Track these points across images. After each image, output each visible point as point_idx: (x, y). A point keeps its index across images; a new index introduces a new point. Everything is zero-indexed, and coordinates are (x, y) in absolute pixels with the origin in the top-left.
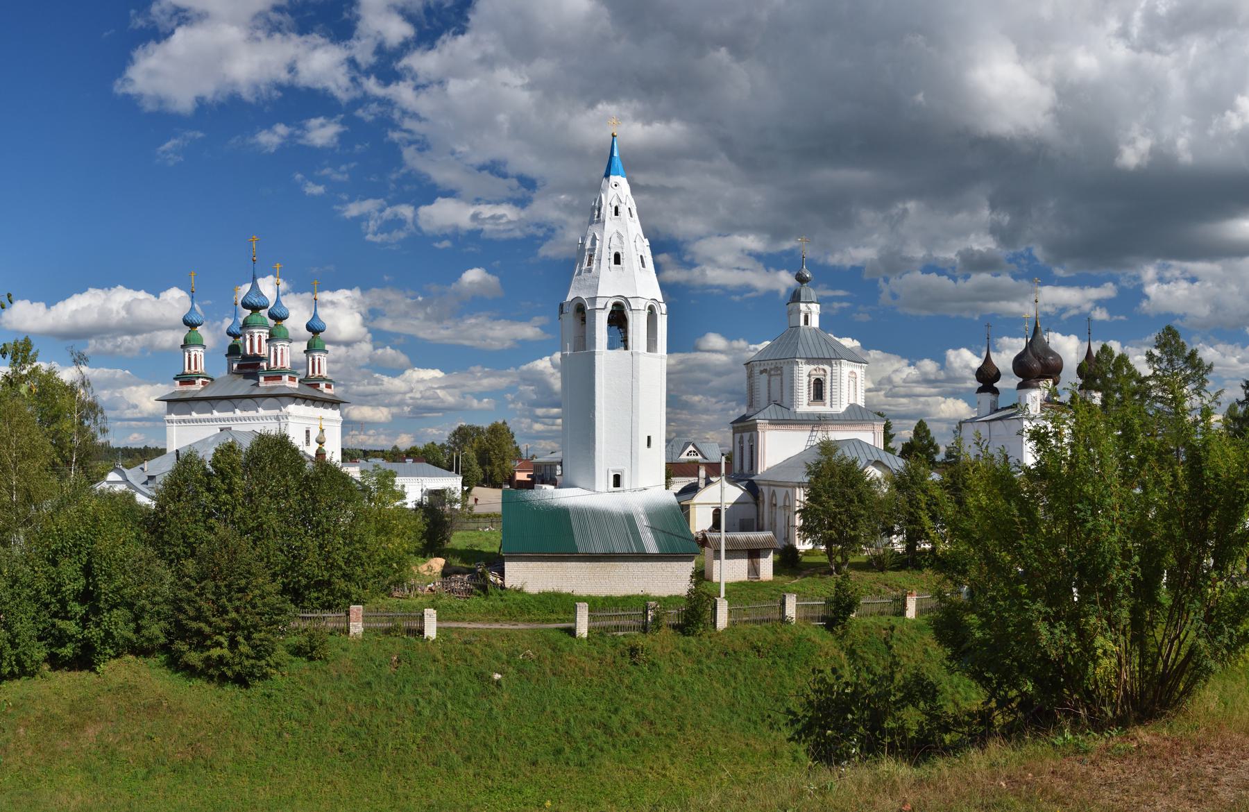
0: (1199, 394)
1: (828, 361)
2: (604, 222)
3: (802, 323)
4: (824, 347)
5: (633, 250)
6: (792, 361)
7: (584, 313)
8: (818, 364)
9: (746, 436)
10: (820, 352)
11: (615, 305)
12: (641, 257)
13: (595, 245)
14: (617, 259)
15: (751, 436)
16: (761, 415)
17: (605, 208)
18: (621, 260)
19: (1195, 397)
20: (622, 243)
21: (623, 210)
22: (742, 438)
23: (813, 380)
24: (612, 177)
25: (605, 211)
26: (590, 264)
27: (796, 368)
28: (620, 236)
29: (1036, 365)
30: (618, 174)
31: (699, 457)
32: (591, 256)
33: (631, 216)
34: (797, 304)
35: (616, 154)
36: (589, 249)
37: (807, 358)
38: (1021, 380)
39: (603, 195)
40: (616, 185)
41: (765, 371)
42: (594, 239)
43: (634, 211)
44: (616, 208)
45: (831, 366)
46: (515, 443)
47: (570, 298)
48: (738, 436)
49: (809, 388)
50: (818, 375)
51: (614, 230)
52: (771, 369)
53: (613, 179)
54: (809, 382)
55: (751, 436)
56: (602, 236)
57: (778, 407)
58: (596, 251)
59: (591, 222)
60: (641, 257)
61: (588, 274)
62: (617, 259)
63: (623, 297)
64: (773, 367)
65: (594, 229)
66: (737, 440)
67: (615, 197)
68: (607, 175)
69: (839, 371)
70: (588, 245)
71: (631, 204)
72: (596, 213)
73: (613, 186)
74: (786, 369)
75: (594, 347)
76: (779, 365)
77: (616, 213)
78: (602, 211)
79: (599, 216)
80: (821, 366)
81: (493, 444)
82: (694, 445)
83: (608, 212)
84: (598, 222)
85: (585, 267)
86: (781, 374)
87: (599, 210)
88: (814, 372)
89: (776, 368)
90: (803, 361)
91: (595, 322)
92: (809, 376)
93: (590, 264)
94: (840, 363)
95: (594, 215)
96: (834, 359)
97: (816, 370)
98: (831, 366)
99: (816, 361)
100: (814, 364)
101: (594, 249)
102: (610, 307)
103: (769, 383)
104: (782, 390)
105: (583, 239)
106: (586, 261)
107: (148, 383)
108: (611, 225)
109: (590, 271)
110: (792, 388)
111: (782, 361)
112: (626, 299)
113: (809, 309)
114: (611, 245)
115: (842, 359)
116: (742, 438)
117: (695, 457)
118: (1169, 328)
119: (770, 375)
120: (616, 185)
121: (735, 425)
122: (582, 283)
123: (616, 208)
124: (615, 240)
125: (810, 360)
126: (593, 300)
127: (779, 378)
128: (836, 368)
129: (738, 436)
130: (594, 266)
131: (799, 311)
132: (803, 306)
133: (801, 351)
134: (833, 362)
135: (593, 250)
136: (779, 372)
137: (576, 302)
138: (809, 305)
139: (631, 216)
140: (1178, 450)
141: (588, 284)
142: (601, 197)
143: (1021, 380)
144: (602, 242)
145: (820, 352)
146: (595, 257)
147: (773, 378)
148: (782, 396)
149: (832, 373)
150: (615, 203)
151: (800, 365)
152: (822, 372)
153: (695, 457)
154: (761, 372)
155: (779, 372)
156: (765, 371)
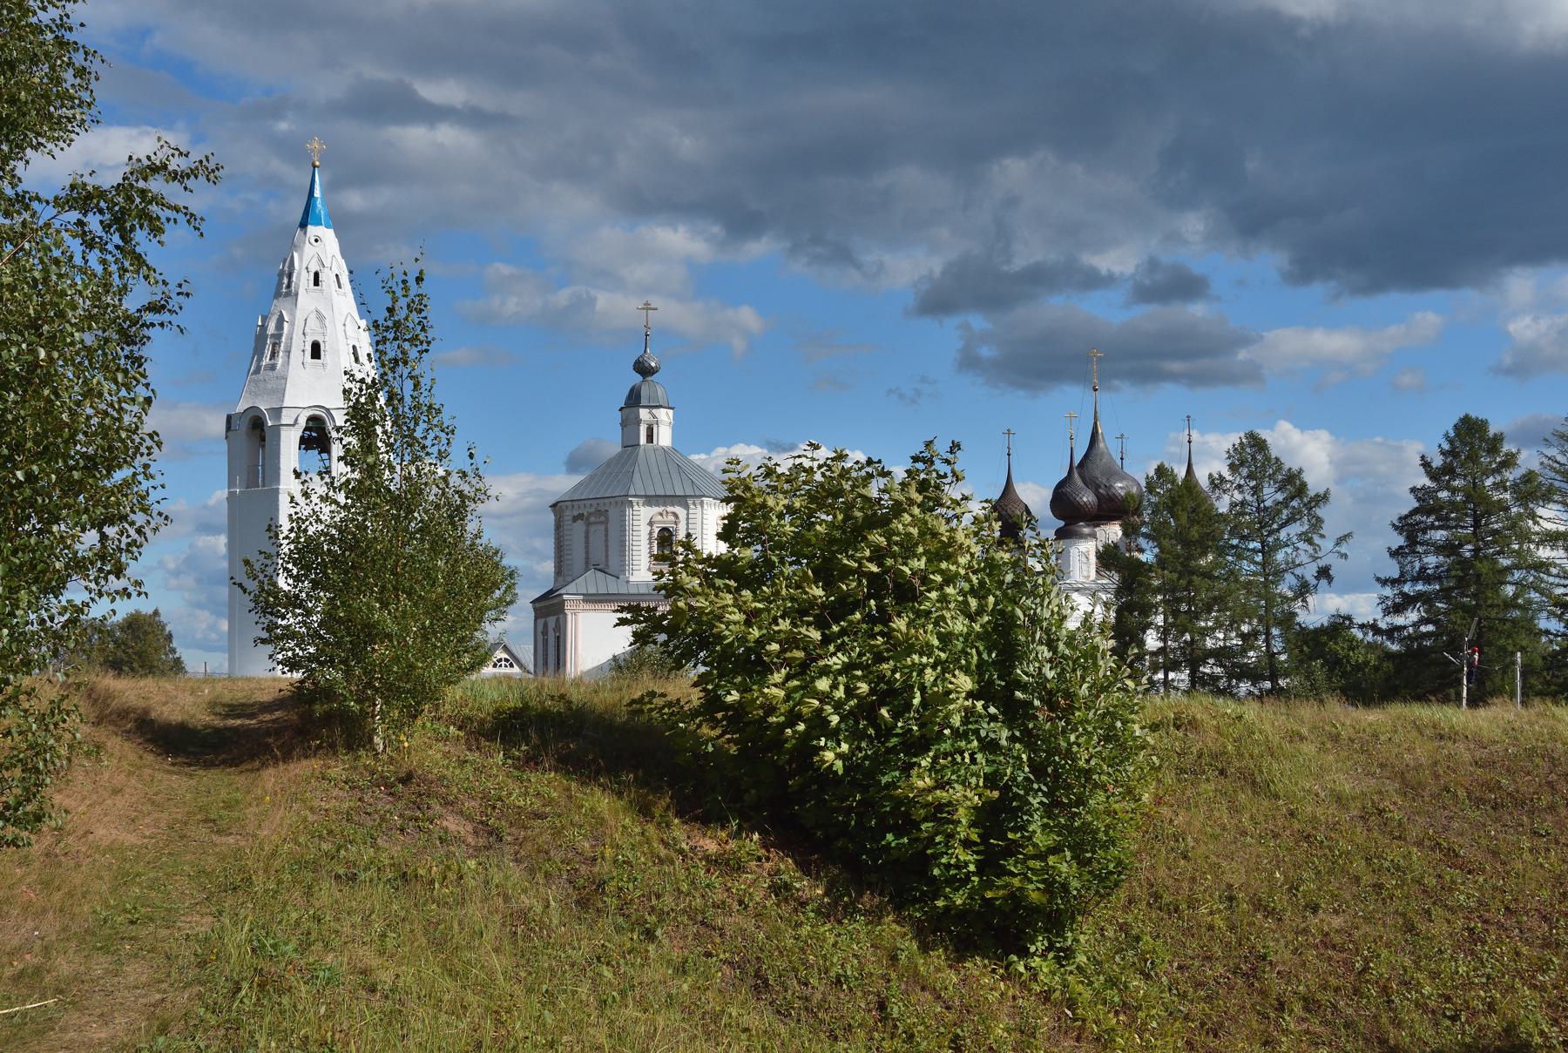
0: (1310, 541)
1: (682, 500)
2: (297, 295)
3: (643, 440)
4: (675, 477)
5: (341, 336)
6: (623, 502)
7: (263, 430)
8: (665, 505)
9: (552, 621)
10: (668, 486)
11: (311, 419)
12: (354, 347)
13: (282, 329)
14: (316, 351)
15: (558, 620)
16: (571, 588)
17: (299, 274)
18: (322, 353)
19: (1302, 545)
20: (324, 326)
21: (327, 278)
22: (545, 625)
23: (657, 530)
24: (310, 228)
25: (299, 278)
26: (273, 355)
27: (628, 511)
28: (321, 317)
29: (1087, 498)
30: (319, 223)
31: (516, 669)
32: (274, 345)
33: (340, 287)
34: (634, 409)
35: (317, 193)
36: (272, 336)
37: (646, 496)
38: (1061, 523)
39: (295, 255)
40: (316, 241)
41: (580, 516)
42: (281, 320)
43: (345, 279)
44: (316, 275)
45: (687, 507)
46: (173, 651)
47: (241, 408)
48: (541, 622)
49: (650, 543)
50: (664, 522)
51: (312, 308)
52: (590, 514)
53: (312, 230)
54: (651, 533)
55: (558, 620)
56: (293, 315)
57: (600, 574)
58: (283, 339)
59: (278, 295)
60: (354, 347)
61: (270, 373)
62: (316, 351)
63: (323, 407)
64: (593, 510)
65: (281, 305)
66: (540, 628)
67: (316, 259)
68: (303, 225)
69: (699, 516)
70: (271, 329)
71: (339, 267)
72: (286, 281)
73: (313, 242)
74: (612, 513)
75: (279, 484)
76: (602, 508)
77: (316, 282)
78: (294, 279)
79: (289, 286)
80: (670, 509)
81: (130, 651)
82: (506, 649)
83: (303, 280)
84: (288, 294)
85: (266, 361)
86: (606, 522)
87: (290, 276)
88: (660, 518)
89: (599, 513)
90: (641, 501)
91: (279, 445)
92: (651, 524)
93: (273, 355)
94: (702, 504)
95: (283, 287)
96: (691, 496)
97: (661, 514)
98: (687, 507)
99: (661, 500)
100: (658, 506)
101: (281, 335)
102: (302, 422)
103: (587, 537)
104: (607, 546)
105: (265, 319)
106: (268, 353)
107: (1308, 429)
108: (307, 299)
109: (273, 367)
110: (622, 544)
111: (606, 501)
112: (328, 410)
113: (654, 417)
114: (307, 330)
115: (704, 496)
116: (545, 625)
117: (509, 670)
118: (1466, 420)
119: (589, 524)
120: (316, 241)
121: (538, 605)
122: (261, 385)
123: (316, 275)
124: (313, 323)
125: (651, 500)
126: (277, 412)
127: (602, 528)
128: (695, 511)
129: (541, 622)
130: (280, 361)
131: (638, 422)
132: (644, 414)
133: (638, 487)
134: (690, 502)
135: (278, 336)
136: (602, 518)
137: (252, 414)
138: (654, 411)
139: (340, 287)
140: (1268, 634)
141: (269, 386)
142: (292, 257)
143: (1061, 523)
144: (292, 324)
145: (668, 486)
146: (282, 348)
147: (592, 528)
148: (607, 556)
149: (688, 519)
150: (313, 268)
151: (636, 508)
152: (672, 518)
153: (509, 670)
154: (575, 519)
155: (602, 518)
156: (580, 516)
